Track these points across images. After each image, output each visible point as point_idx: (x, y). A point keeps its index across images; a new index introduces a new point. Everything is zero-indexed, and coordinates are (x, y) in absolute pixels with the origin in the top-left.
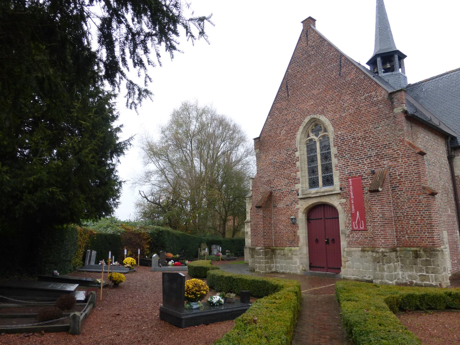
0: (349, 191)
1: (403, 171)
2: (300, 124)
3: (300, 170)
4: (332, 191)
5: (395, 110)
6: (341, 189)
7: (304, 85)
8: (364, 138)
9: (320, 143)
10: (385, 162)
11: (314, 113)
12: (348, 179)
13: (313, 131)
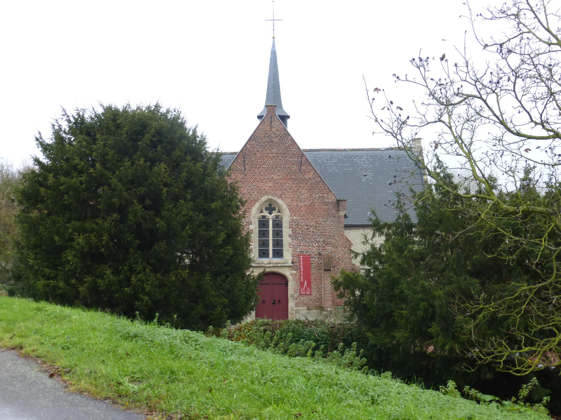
0: (300, 265)
1: (341, 256)
2: (256, 201)
3: (253, 241)
4: (284, 263)
5: (340, 213)
6: (293, 263)
7: (264, 166)
8: (316, 227)
9: (273, 220)
10: (329, 248)
11: (272, 195)
12: (299, 256)
13: (266, 209)
